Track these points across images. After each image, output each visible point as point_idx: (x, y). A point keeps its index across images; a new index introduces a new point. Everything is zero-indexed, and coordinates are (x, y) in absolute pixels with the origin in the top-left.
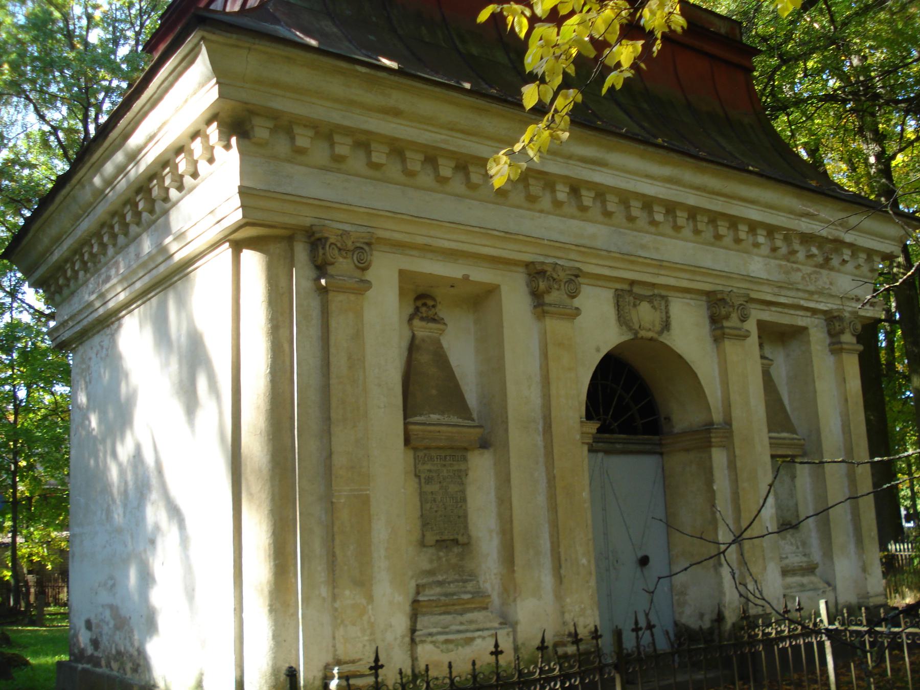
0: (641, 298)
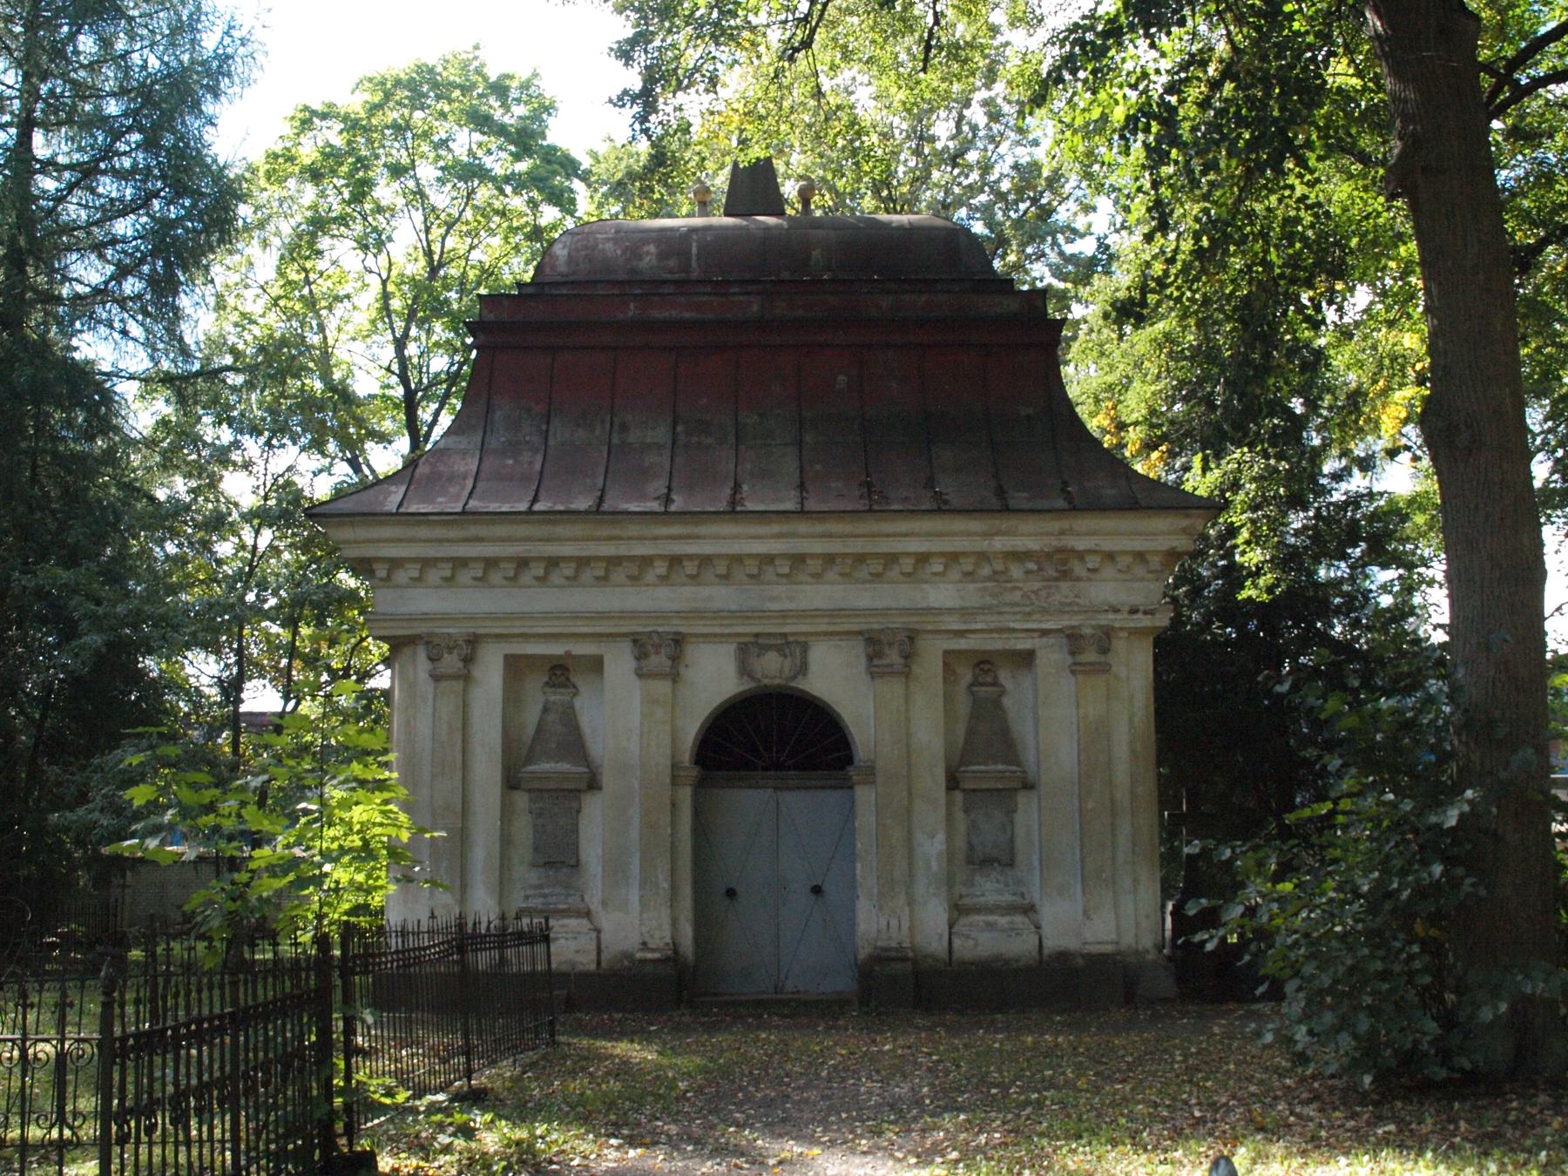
0: (769, 648)
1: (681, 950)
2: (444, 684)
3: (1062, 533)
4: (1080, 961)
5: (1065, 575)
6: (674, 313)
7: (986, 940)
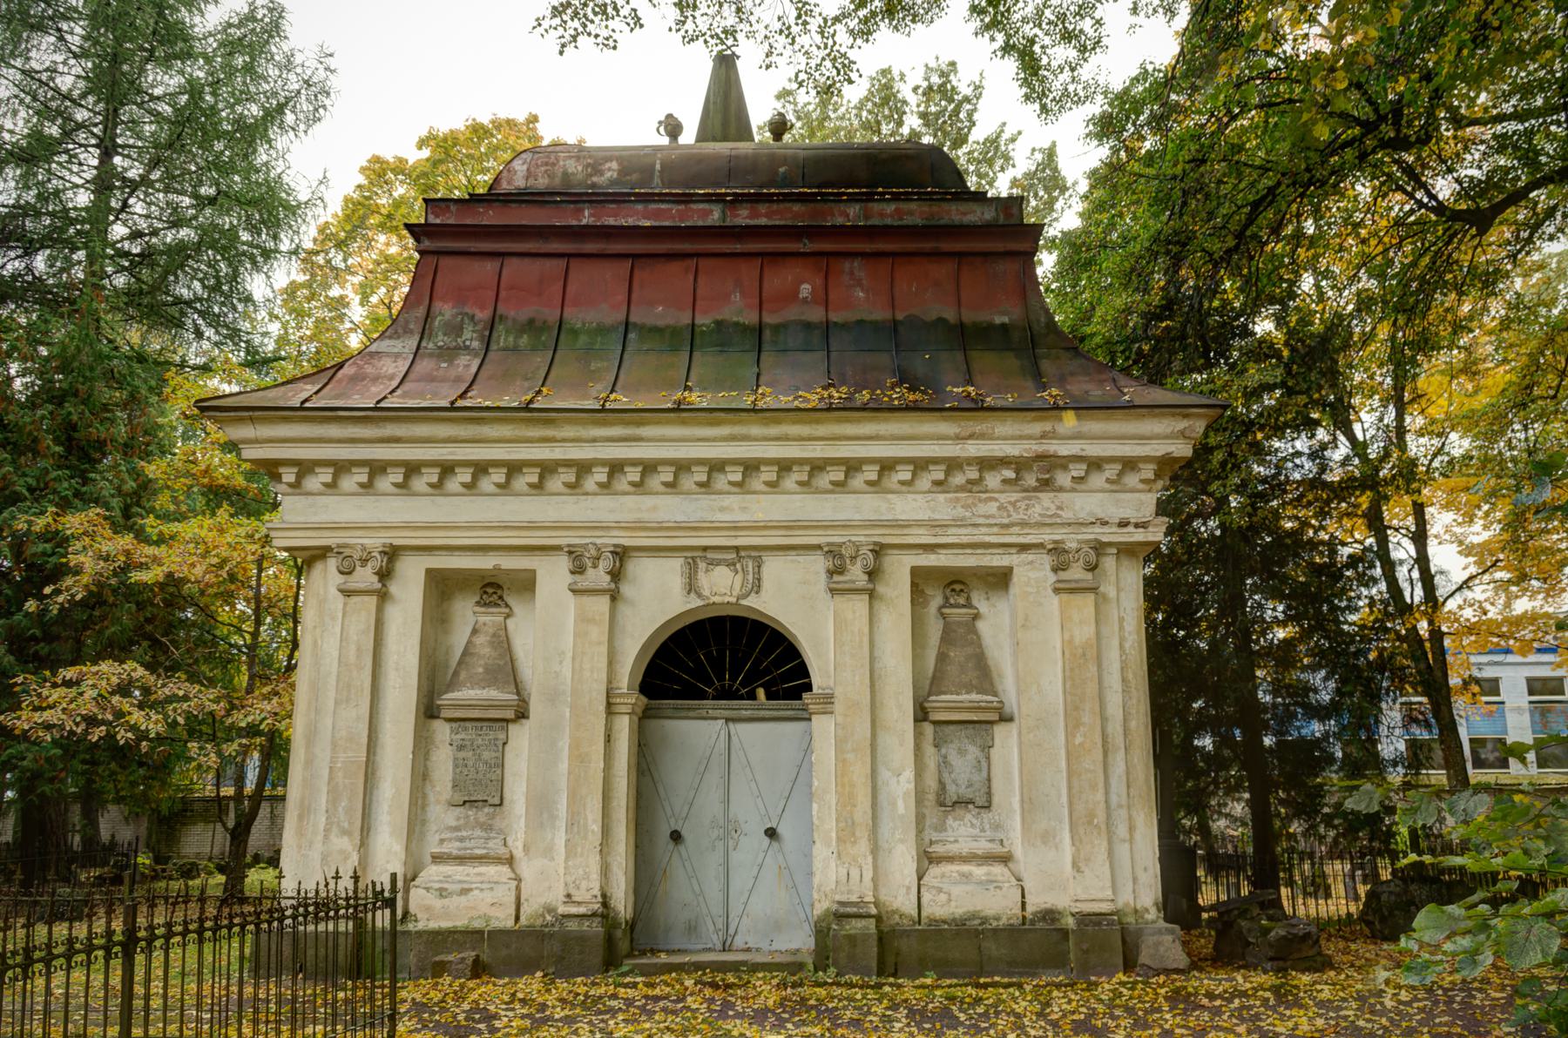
1: (612, 903)
2: (354, 599)
3: (1044, 436)
4: (1070, 922)
5: (1046, 484)
6: (631, 222)
7: (960, 895)
